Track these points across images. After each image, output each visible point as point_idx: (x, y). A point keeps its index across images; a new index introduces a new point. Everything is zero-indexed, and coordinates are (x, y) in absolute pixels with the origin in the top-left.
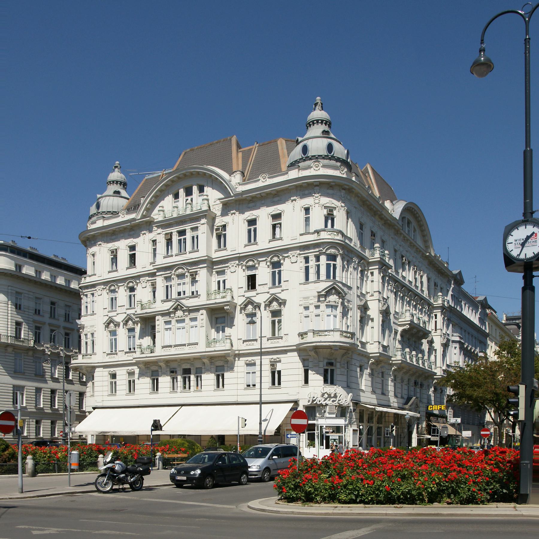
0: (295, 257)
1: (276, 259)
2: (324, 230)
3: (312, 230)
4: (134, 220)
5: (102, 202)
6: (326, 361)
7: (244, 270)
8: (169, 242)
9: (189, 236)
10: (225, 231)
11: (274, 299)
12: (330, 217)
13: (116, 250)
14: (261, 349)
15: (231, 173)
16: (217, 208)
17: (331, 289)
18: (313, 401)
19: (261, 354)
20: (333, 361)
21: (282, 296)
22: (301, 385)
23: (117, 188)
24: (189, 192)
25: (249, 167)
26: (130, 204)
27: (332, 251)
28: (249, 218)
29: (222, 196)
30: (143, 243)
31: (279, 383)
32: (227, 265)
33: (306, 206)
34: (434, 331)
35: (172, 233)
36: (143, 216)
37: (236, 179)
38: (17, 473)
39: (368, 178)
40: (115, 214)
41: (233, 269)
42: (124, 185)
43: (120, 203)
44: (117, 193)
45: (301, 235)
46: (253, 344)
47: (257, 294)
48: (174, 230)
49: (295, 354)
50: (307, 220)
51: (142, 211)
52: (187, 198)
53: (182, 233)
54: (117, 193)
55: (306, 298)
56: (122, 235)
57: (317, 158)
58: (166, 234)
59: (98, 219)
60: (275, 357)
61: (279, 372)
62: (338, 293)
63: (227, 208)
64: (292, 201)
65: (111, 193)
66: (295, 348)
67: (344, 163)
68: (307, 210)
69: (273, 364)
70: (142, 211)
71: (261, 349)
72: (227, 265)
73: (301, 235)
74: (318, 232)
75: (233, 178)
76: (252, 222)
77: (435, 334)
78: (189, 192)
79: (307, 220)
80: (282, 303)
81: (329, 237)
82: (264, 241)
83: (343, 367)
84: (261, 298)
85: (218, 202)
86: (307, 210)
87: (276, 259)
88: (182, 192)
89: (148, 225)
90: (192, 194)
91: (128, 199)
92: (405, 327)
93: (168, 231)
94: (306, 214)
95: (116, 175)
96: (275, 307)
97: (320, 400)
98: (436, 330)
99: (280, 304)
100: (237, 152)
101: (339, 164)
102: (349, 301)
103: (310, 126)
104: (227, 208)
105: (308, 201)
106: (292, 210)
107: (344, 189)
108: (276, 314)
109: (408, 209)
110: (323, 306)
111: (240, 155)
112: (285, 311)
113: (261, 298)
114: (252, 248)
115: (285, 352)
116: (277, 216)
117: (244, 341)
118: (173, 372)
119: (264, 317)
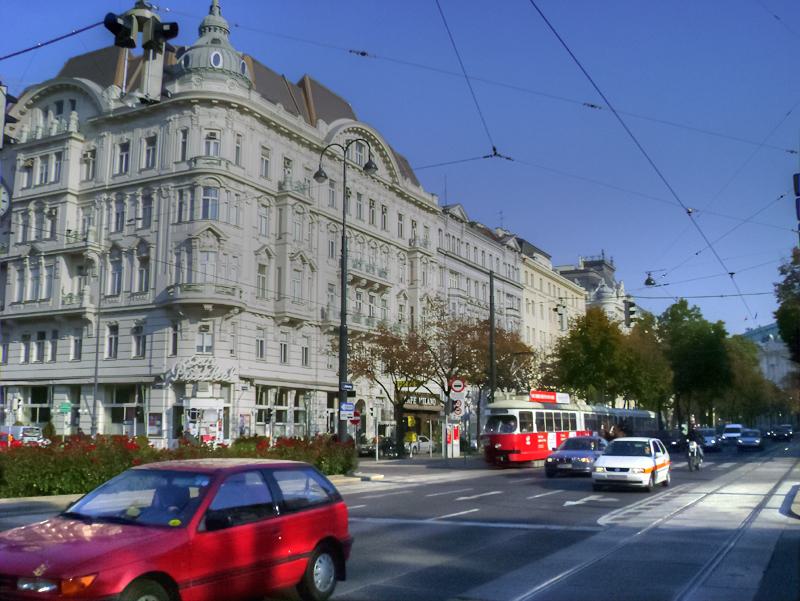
108: (145, 262)
118: (26, 339)
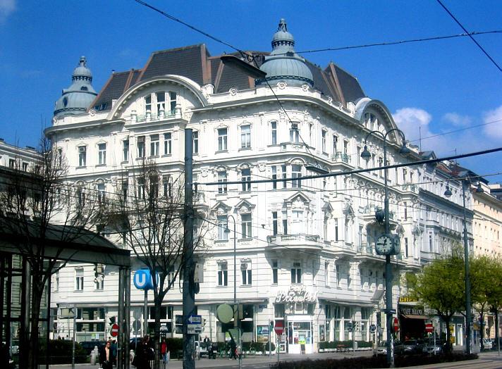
0: (263, 167)
1: (245, 167)
2: (290, 144)
3: (278, 143)
4: (106, 120)
5: (69, 97)
6: (293, 262)
7: (215, 176)
8: (141, 144)
9: (162, 140)
10: (197, 137)
11: (245, 203)
12: (295, 128)
13: (85, 147)
14: (235, 249)
15: (202, 85)
16: (189, 116)
17: (297, 197)
18: (282, 299)
19: (235, 254)
20: (300, 262)
21: (252, 201)
22: (271, 284)
23: (83, 83)
24: (161, 98)
25: (219, 77)
26: (99, 99)
27: (298, 162)
28: (220, 127)
29: (192, 106)
30: (114, 142)
31: (250, 282)
32: (198, 169)
33: (273, 121)
34: (404, 219)
35: (144, 136)
36: (115, 118)
37: (208, 90)
38: (362, 318)
39: (331, 77)
40: (84, 111)
41: (204, 174)
42: (89, 79)
43: (87, 99)
44: (84, 89)
45: (269, 146)
46: (224, 245)
47: (228, 198)
48: (147, 134)
49: (263, 255)
50: (274, 134)
51: (113, 112)
52: (159, 103)
53: (155, 137)
54: (84, 89)
55: (274, 204)
56: (92, 133)
57: (282, 78)
58: (139, 137)
59: (66, 115)
60: (246, 257)
61: (250, 272)
62: (303, 200)
63: (197, 116)
64: (260, 115)
65: (79, 89)
66: (264, 249)
67: (307, 81)
68: (274, 124)
69: (244, 267)
70: (113, 112)
71: (235, 249)
72: (198, 169)
73: (269, 146)
74: (284, 145)
75: (203, 90)
76: (223, 131)
77: (405, 222)
78: (161, 98)
79: (274, 134)
80: (251, 207)
81: (294, 150)
82: (234, 152)
83: (309, 267)
84: (232, 202)
85: (190, 110)
86: (274, 124)
87: (245, 165)
88: (154, 97)
89: (119, 125)
90: (164, 100)
91: (96, 95)
92: (370, 222)
93: (140, 134)
94: (273, 128)
95: (82, 70)
96: (245, 211)
97: (288, 298)
98: (406, 218)
99: (250, 209)
100: (207, 60)
101: (301, 82)
102: (313, 206)
103: (275, 45)
104: (197, 116)
105: (274, 116)
106: (260, 124)
107: (307, 105)
108: (246, 217)
109: (373, 107)
110: (289, 212)
111: (209, 63)
112: (254, 213)
113: (232, 202)
114: (222, 156)
115: (255, 253)
116: (102, 146)
117: (215, 242)
119: (235, 220)
